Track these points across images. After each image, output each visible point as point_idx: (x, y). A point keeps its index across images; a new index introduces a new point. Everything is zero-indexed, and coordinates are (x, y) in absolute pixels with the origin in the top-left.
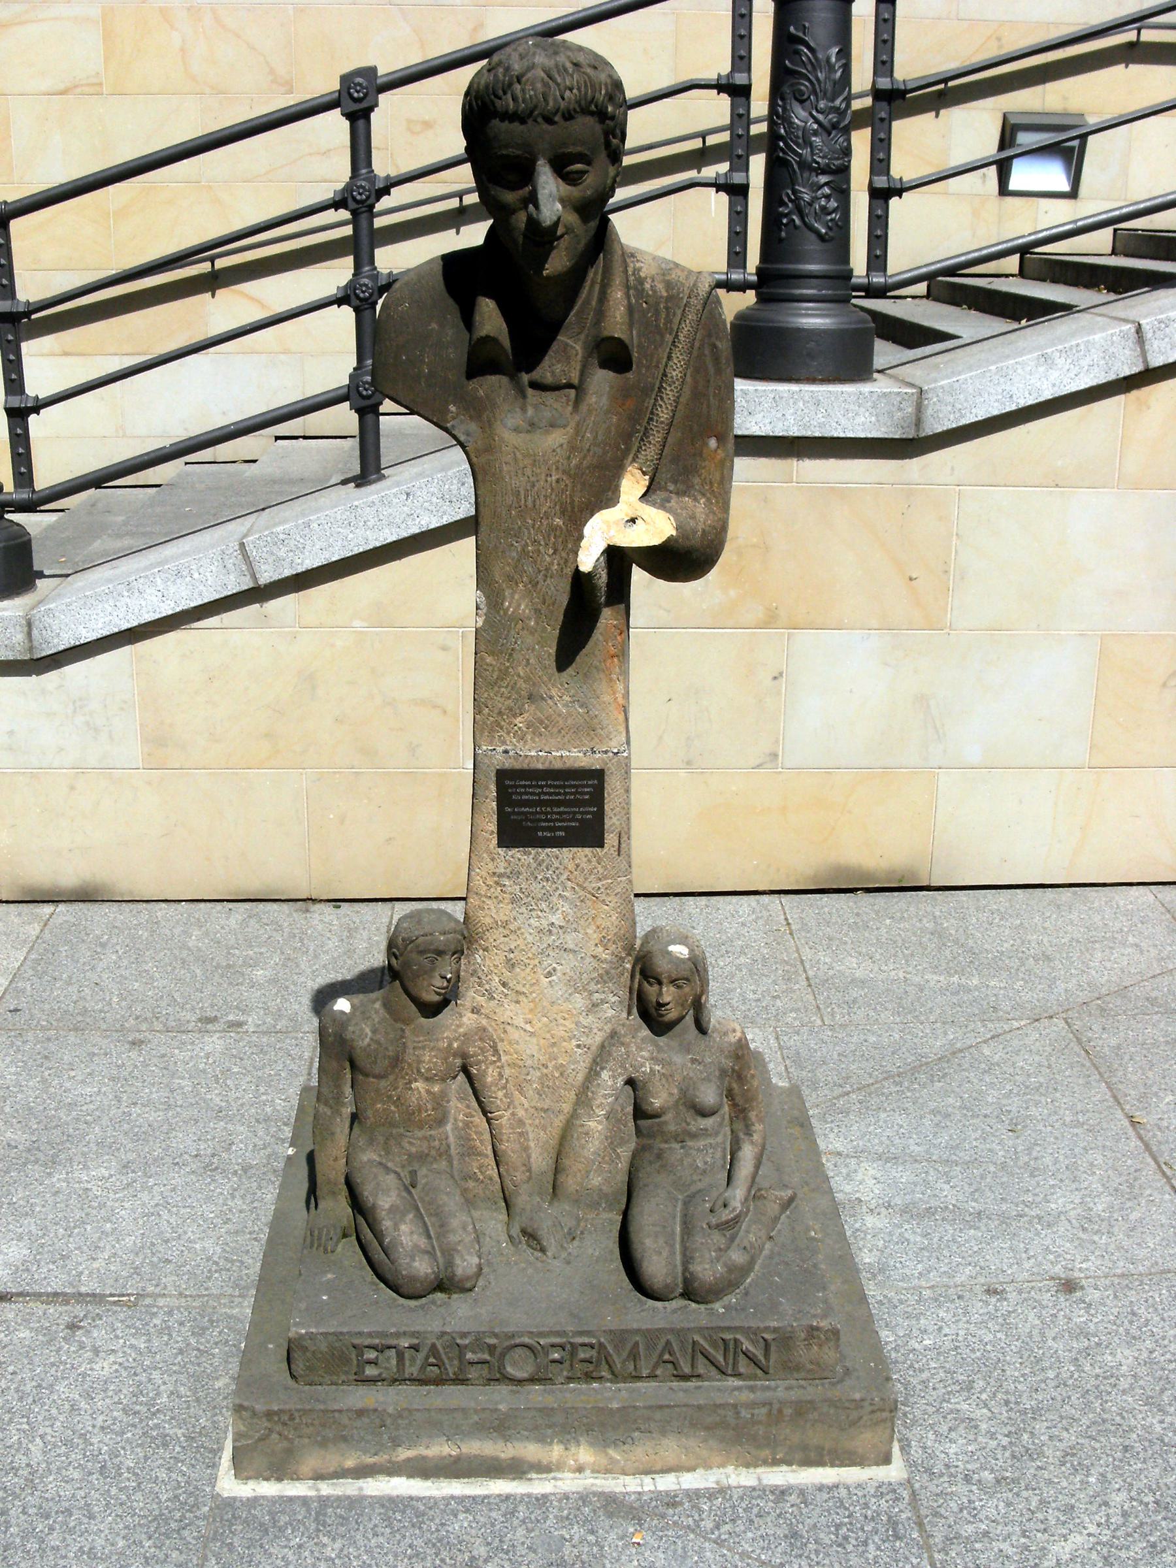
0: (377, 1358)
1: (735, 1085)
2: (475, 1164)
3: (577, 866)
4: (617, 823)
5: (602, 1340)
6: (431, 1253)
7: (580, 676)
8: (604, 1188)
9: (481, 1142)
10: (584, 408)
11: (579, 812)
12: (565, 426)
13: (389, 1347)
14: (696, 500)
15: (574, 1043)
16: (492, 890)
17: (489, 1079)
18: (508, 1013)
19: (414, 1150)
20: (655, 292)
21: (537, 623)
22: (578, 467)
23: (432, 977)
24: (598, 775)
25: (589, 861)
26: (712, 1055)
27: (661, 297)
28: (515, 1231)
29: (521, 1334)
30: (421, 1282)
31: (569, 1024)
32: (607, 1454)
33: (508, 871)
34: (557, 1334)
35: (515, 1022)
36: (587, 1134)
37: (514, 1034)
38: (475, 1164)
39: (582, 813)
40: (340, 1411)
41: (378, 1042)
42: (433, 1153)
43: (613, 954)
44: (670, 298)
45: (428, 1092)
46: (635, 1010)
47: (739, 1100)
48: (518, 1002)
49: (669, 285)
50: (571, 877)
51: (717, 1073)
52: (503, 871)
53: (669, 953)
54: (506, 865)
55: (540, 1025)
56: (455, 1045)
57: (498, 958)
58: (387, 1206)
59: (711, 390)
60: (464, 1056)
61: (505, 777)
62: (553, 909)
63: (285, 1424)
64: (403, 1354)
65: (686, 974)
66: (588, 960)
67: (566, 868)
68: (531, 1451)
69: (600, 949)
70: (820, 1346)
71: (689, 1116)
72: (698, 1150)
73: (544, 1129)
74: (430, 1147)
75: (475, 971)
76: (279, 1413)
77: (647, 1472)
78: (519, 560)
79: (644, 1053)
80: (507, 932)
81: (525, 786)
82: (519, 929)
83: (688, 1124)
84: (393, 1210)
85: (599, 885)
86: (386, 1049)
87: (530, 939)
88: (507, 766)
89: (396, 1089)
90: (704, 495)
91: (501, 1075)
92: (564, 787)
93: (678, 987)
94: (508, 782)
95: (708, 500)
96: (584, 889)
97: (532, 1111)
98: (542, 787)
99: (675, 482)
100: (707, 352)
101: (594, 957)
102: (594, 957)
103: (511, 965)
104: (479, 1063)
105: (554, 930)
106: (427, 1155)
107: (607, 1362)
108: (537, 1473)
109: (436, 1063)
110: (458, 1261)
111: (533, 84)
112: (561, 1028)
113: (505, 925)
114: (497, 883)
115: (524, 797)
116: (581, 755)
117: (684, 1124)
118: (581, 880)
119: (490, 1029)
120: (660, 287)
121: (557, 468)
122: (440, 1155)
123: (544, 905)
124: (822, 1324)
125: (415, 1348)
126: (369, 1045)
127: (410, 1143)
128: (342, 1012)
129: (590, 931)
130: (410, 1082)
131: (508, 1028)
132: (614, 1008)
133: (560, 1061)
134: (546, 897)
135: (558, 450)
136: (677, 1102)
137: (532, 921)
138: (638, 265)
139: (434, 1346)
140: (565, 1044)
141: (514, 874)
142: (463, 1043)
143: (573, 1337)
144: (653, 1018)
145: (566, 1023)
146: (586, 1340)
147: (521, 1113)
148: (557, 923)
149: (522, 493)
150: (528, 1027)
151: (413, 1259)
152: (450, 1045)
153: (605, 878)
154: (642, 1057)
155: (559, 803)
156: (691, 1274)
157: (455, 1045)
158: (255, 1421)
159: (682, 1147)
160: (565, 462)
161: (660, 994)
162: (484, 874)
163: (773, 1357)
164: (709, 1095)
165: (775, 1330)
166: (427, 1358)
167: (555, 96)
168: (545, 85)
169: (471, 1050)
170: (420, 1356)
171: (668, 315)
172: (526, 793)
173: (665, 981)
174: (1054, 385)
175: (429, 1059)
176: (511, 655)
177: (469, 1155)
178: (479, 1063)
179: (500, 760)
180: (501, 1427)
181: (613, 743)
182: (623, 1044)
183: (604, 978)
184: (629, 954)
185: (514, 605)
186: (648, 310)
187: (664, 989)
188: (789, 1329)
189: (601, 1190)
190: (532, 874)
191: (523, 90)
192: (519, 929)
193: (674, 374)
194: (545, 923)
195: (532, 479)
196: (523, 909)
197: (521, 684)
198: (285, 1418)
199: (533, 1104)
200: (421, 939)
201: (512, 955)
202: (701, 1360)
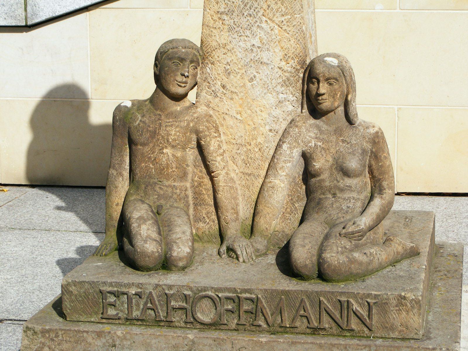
0: (115, 301)
1: (373, 163)
2: (204, 212)
5: (260, 296)
6: (160, 243)
8: (286, 230)
9: (208, 195)
13: (124, 294)
15: (268, 128)
16: (217, 23)
17: (212, 148)
18: (227, 107)
19: (162, 192)
26: (357, 140)
28: (224, 248)
29: (205, 289)
31: (265, 115)
33: (226, 10)
34: (229, 290)
35: (231, 113)
36: (273, 187)
38: (204, 212)
40: (87, 332)
41: (144, 122)
42: (175, 196)
43: (292, 66)
45: (173, 155)
46: (305, 106)
47: (376, 173)
48: (232, 99)
50: (265, 14)
51: (360, 151)
52: (223, 10)
53: (324, 61)
54: (225, 6)
55: (246, 115)
56: (191, 125)
57: (220, 68)
58: (137, 217)
60: (197, 132)
63: (52, 340)
64: (132, 299)
65: (335, 75)
66: (277, 70)
67: (261, 8)
69: (283, 63)
70: (408, 312)
71: (339, 176)
72: (344, 199)
73: (248, 188)
74: (173, 193)
75: (206, 78)
76: (49, 331)
79: (309, 132)
82: (233, 48)
83: (338, 182)
84: (140, 218)
85: (283, 19)
86: (149, 126)
87: (240, 56)
89: (153, 153)
91: (220, 147)
93: (331, 84)
96: (273, 21)
97: (240, 174)
101: (280, 68)
102: (280, 68)
103: (228, 73)
104: (206, 136)
105: (255, 50)
106: (171, 197)
107: (262, 312)
109: (179, 136)
110: (175, 248)
112: (260, 118)
114: (220, 19)
117: (335, 182)
118: (271, 15)
119: (215, 117)
122: (180, 199)
123: (248, 33)
124: (407, 296)
125: (139, 295)
126: (139, 124)
127: (160, 188)
128: (126, 107)
129: (277, 50)
130: (163, 149)
131: (226, 117)
132: (291, 102)
133: (259, 140)
134: (250, 27)
136: (331, 167)
137: (241, 44)
139: (151, 293)
140: (261, 128)
142: (196, 123)
143: (241, 293)
144: (314, 107)
145: (263, 114)
146: (248, 295)
147: (233, 175)
148: (256, 45)
150: (239, 117)
151: (145, 242)
152: (188, 124)
153: (286, 14)
154: (309, 136)
156: (323, 259)
157: (191, 125)
158: (35, 337)
159: (334, 197)
161: (318, 88)
162: (213, 13)
163: (375, 318)
164: (353, 164)
165: (376, 296)
166: (146, 303)
169: (201, 128)
170: (142, 303)
173: (321, 79)
175: (174, 133)
177: (200, 205)
178: (206, 136)
182: (297, 126)
183: (286, 83)
184: (302, 67)
187: (321, 84)
188: (385, 296)
189: (283, 231)
192: (233, 48)
194: (249, 44)
196: (235, 36)
198: (53, 335)
199: (241, 170)
200: (171, 50)
201: (228, 67)
202: (325, 318)
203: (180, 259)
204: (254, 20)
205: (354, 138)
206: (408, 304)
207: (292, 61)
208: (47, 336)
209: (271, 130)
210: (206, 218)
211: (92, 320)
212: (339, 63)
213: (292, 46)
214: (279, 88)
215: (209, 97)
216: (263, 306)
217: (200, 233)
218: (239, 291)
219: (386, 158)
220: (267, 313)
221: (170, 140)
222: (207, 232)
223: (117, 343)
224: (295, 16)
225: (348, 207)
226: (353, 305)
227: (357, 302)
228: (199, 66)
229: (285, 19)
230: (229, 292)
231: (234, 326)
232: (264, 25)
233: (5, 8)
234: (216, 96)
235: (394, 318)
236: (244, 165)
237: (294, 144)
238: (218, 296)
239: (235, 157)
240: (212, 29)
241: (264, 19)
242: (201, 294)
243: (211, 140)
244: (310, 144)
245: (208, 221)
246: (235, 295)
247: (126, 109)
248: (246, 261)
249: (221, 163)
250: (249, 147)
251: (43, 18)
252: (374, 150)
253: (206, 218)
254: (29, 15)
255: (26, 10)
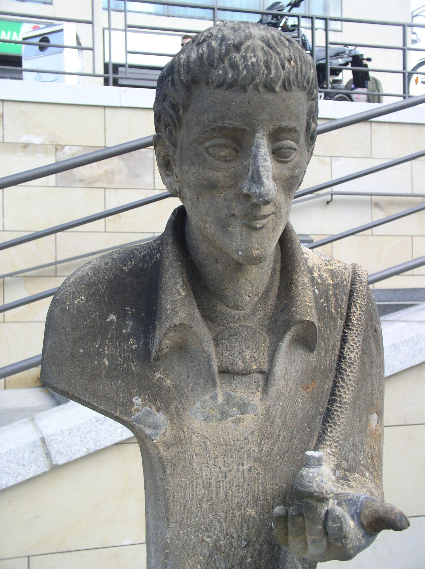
10: (272, 392)
14: (364, 475)
20: (323, 280)
22: (269, 452)
27: (329, 285)
44: (336, 286)
49: (333, 274)
78: (210, 556)
100: (370, 335)
111: (254, 51)
120: (325, 275)
121: (249, 456)
135: (249, 438)
149: (214, 483)
160: (256, 449)
167: (276, 64)
168: (265, 53)
171: (336, 300)
174: (401, 363)
191: (245, 58)
193: (352, 356)
195: (224, 469)
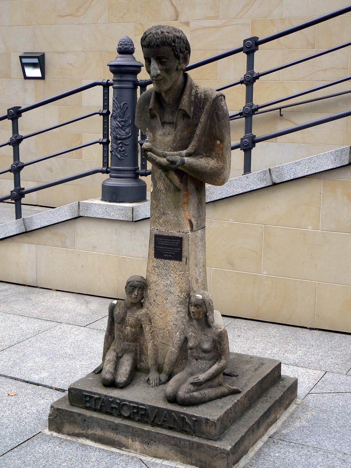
3: (175, 266)
4: (186, 255)
7: (176, 208)
11: (175, 250)
12: (172, 135)
21: (165, 192)
22: (175, 146)
23: (132, 294)
24: (181, 239)
25: (178, 265)
26: (211, 334)
29: (125, 401)
30: (107, 381)
32: (143, 446)
33: (157, 266)
37: (157, 318)
38: (144, 358)
39: (176, 250)
42: (130, 350)
44: (205, 99)
48: (158, 307)
49: (205, 95)
51: (212, 340)
53: (196, 296)
59: (216, 126)
61: (156, 236)
62: (168, 279)
67: (171, 267)
68: (122, 439)
77: (155, 457)
80: (156, 285)
81: (161, 240)
82: (159, 284)
88: (158, 234)
90: (216, 158)
92: (171, 242)
93: (198, 308)
94: (157, 239)
95: (217, 159)
98: (166, 241)
99: (206, 153)
101: (178, 296)
102: (178, 296)
105: (168, 286)
106: (128, 350)
108: (125, 448)
113: (155, 282)
115: (161, 244)
116: (176, 232)
117: (198, 354)
118: (175, 271)
119: (150, 314)
123: (165, 277)
130: (126, 327)
131: (155, 315)
134: (166, 275)
135: (170, 141)
137: (162, 282)
138: (197, 89)
141: (158, 267)
155: (170, 246)
167: (154, 41)
172: (162, 242)
176: (159, 200)
179: (156, 232)
180: (115, 428)
181: (185, 230)
185: (160, 186)
186: (198, 102)
190: (163, 267)
197: (161, 210)
198: (61, 411)
203: (121, 383)
204: (168, 272)
205: (209, 333)
206: (210, 423)
207: (184, 293)
208: (59, 411)
209: (174, 324)
210: (144, 361)
211: (80, 406)
212: (202, 298)
213: (184, 286)
214: (178, 305)
215: (148, 305)
216: (149, 413)
217: (141, 368)
218: (139, 404)
219: (224, 344)
220: (150, 416)
221: (129, 323)
222: (144, 368)
223: (87, 420)
224: (186, 272)
225: (202, 367)
226: (186, 419)
227: (188, 418)
228: (144, 289)
229: (181, 273)
230: (135, 404)
231: (137, 420)
232: (172, 275)
233: (123, 212)
234: (151, 305)
235: (204, 429)
236: (162, 339)
237: (182, 333)
238: (130, 405)
239: (158, 334)
240: (150, 274)
241: (172, 272)
242: (123, 403)
243: (147, 326)
244: (189, 334)
245: (145, 362)
246: (137, 405)
247: (114, 305)
248: (153, 386)
249: (151, 337)
250: (164, 331)
251: (141, 218)
252: (219, 340)
253: (144, 361)
254: (134, 216)
255: (133, 213)
